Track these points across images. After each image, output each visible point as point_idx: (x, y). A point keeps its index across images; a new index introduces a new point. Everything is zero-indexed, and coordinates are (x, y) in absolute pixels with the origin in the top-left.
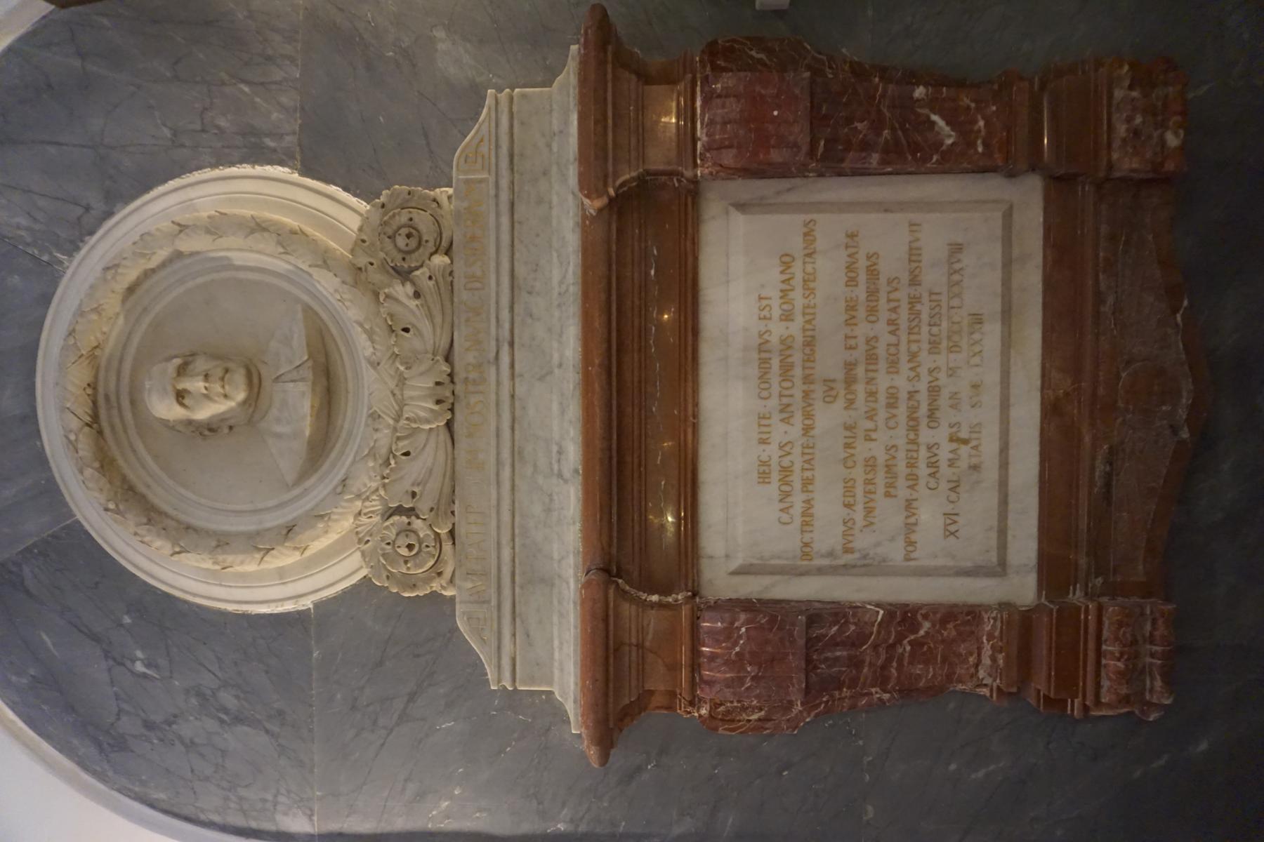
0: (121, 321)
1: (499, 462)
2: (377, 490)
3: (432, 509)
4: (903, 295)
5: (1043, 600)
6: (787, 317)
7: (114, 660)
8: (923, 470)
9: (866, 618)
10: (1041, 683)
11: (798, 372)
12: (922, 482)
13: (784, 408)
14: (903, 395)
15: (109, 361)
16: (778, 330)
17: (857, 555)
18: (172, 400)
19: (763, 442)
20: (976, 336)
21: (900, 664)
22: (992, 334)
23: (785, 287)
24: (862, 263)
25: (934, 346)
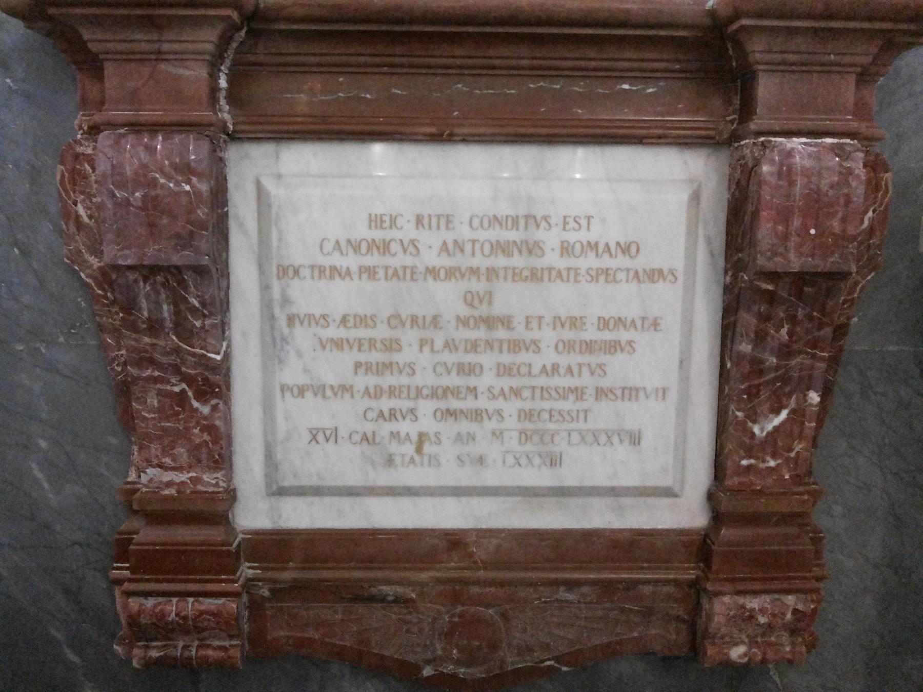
4: (585, 380)
5: (241, 536)
6: (566, 249)
8: (386, 404)
9: (211, 341)
10: (148, 535)
11: (501, 261)
12: (373, 403)
14: (472, 381)
16: (551, 238)
17: (286, 331)
19: (419, 220)
20: (537, 461)
21: (156, 380)
22: (535, 476)
23: (601, 247)
24: (624, 336)
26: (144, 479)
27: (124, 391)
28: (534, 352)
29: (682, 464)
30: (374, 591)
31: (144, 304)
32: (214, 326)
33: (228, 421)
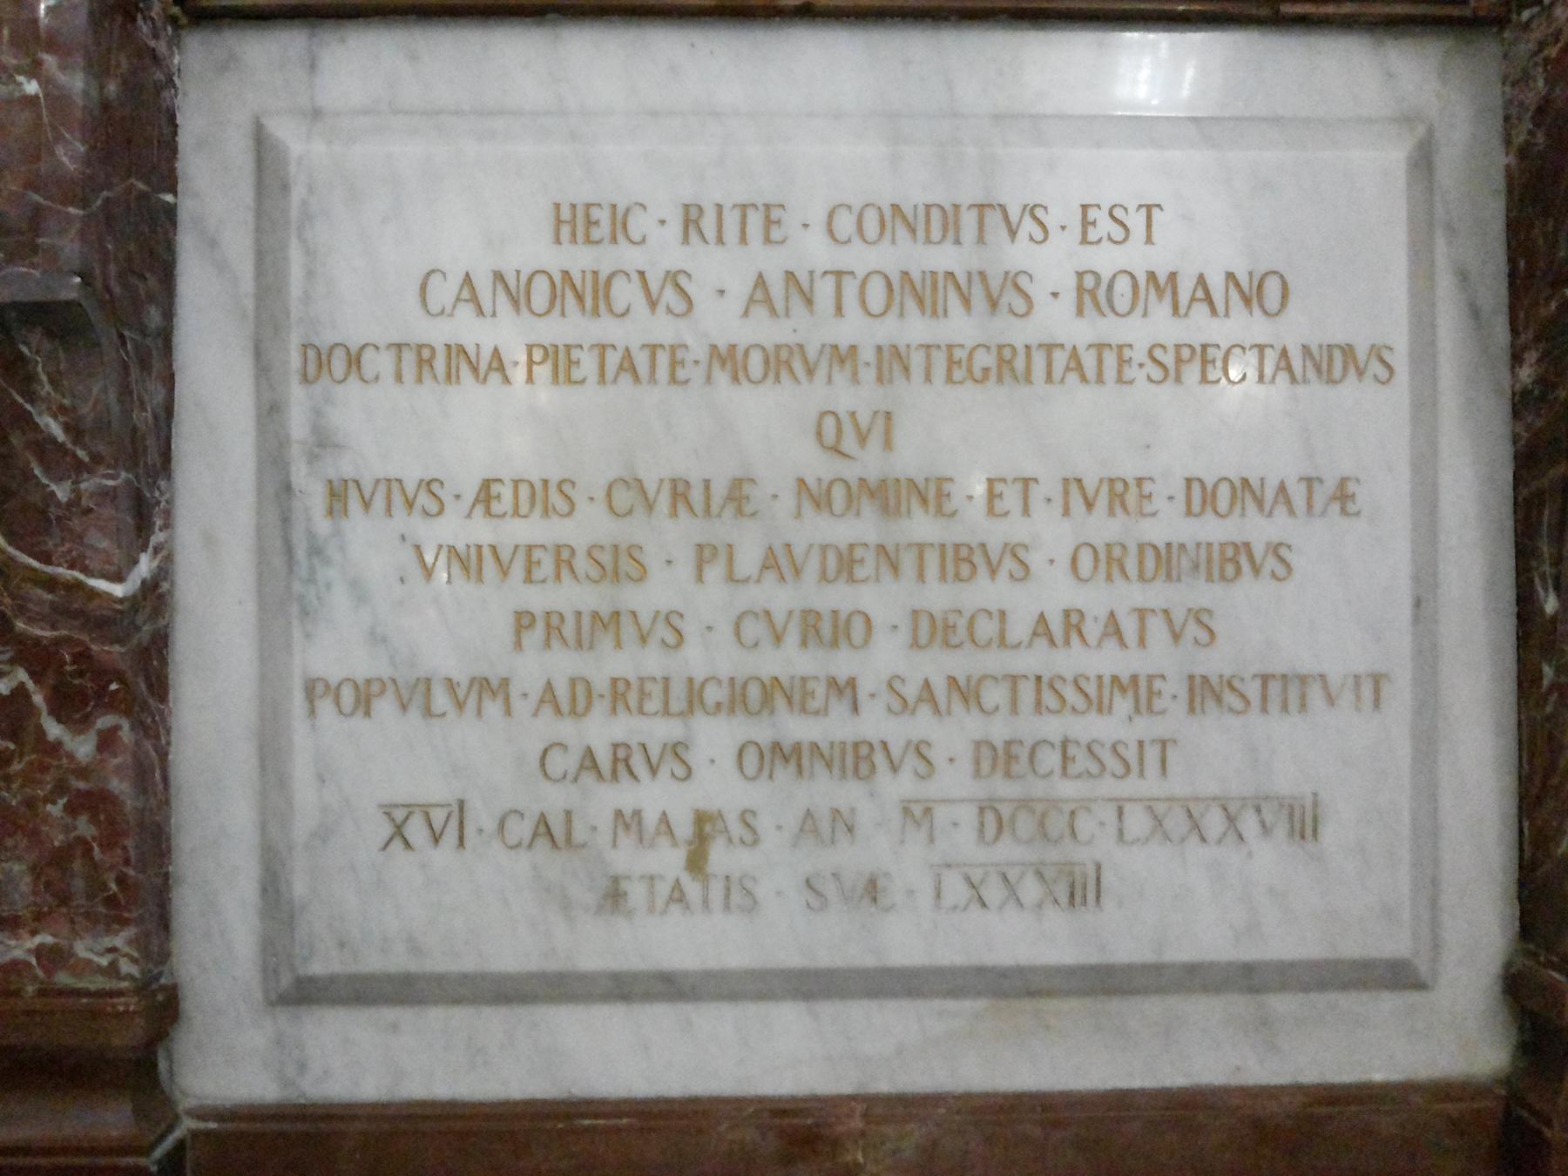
4: (1160, 657)
5: (188, 1124)
6: (1091, 293)
11: (914, 329)
12: (565, 729)
14: (843, 664)
16: (1051, 264)
17: (323, 526)
19: (691, 219)
20: (1031, 890)
23: (1186, 288)
24: (1258, 529)
25: (1000, 758)
29: (1429, 886)
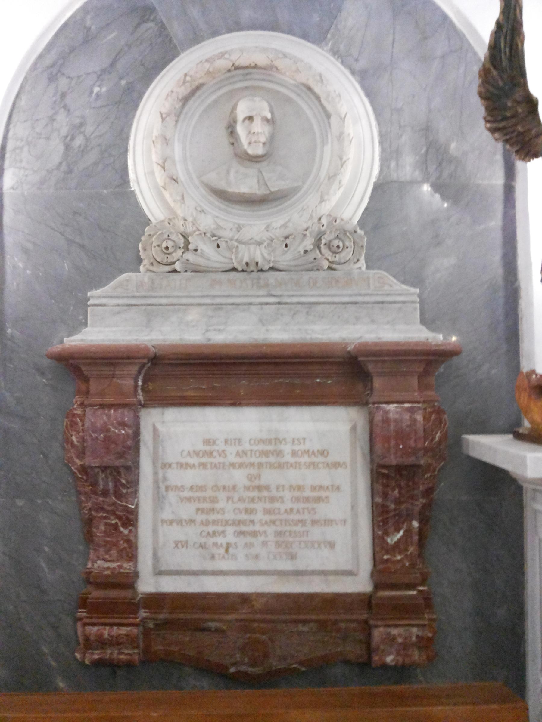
0: (292, 82)
1: (214, 297)
2: (199, 230)
3: (188, 260)
4: (307, 516)
5: (140, 596)
6: (294, 453)
7: (100, 75)
8: (211, 529)
9: (130, 499)
10: (97, 594)
11: (264, 460)
12: (205, 528)
13: (245, 453)
14: (252, 517)
15: (270, 75)
16: (287, 448)
17: (164, 493)
18: (248, 141)
19: (226, 441)
20: (284, 557)
21: (105, 518)
22: (287, 565)
23: (310, 453)
24: (323, 494)
25: (279, 534)
26: (96, 566)
27: (89, 523)
28: (281, 503)
29: (356, 558)
30: (205, 625)
31: (101, 482)
32: (132, 492)
33: (136, 536)
